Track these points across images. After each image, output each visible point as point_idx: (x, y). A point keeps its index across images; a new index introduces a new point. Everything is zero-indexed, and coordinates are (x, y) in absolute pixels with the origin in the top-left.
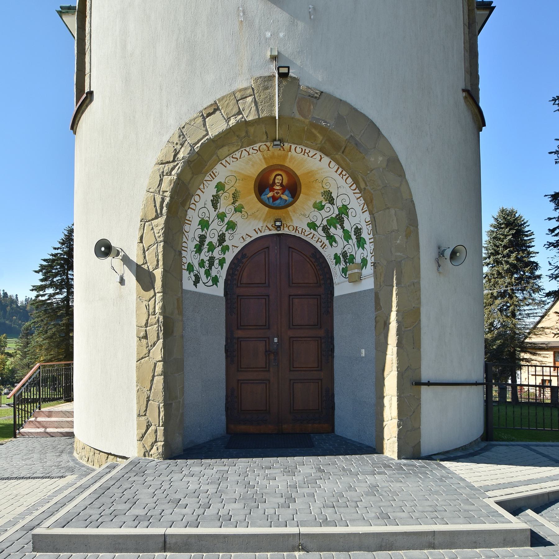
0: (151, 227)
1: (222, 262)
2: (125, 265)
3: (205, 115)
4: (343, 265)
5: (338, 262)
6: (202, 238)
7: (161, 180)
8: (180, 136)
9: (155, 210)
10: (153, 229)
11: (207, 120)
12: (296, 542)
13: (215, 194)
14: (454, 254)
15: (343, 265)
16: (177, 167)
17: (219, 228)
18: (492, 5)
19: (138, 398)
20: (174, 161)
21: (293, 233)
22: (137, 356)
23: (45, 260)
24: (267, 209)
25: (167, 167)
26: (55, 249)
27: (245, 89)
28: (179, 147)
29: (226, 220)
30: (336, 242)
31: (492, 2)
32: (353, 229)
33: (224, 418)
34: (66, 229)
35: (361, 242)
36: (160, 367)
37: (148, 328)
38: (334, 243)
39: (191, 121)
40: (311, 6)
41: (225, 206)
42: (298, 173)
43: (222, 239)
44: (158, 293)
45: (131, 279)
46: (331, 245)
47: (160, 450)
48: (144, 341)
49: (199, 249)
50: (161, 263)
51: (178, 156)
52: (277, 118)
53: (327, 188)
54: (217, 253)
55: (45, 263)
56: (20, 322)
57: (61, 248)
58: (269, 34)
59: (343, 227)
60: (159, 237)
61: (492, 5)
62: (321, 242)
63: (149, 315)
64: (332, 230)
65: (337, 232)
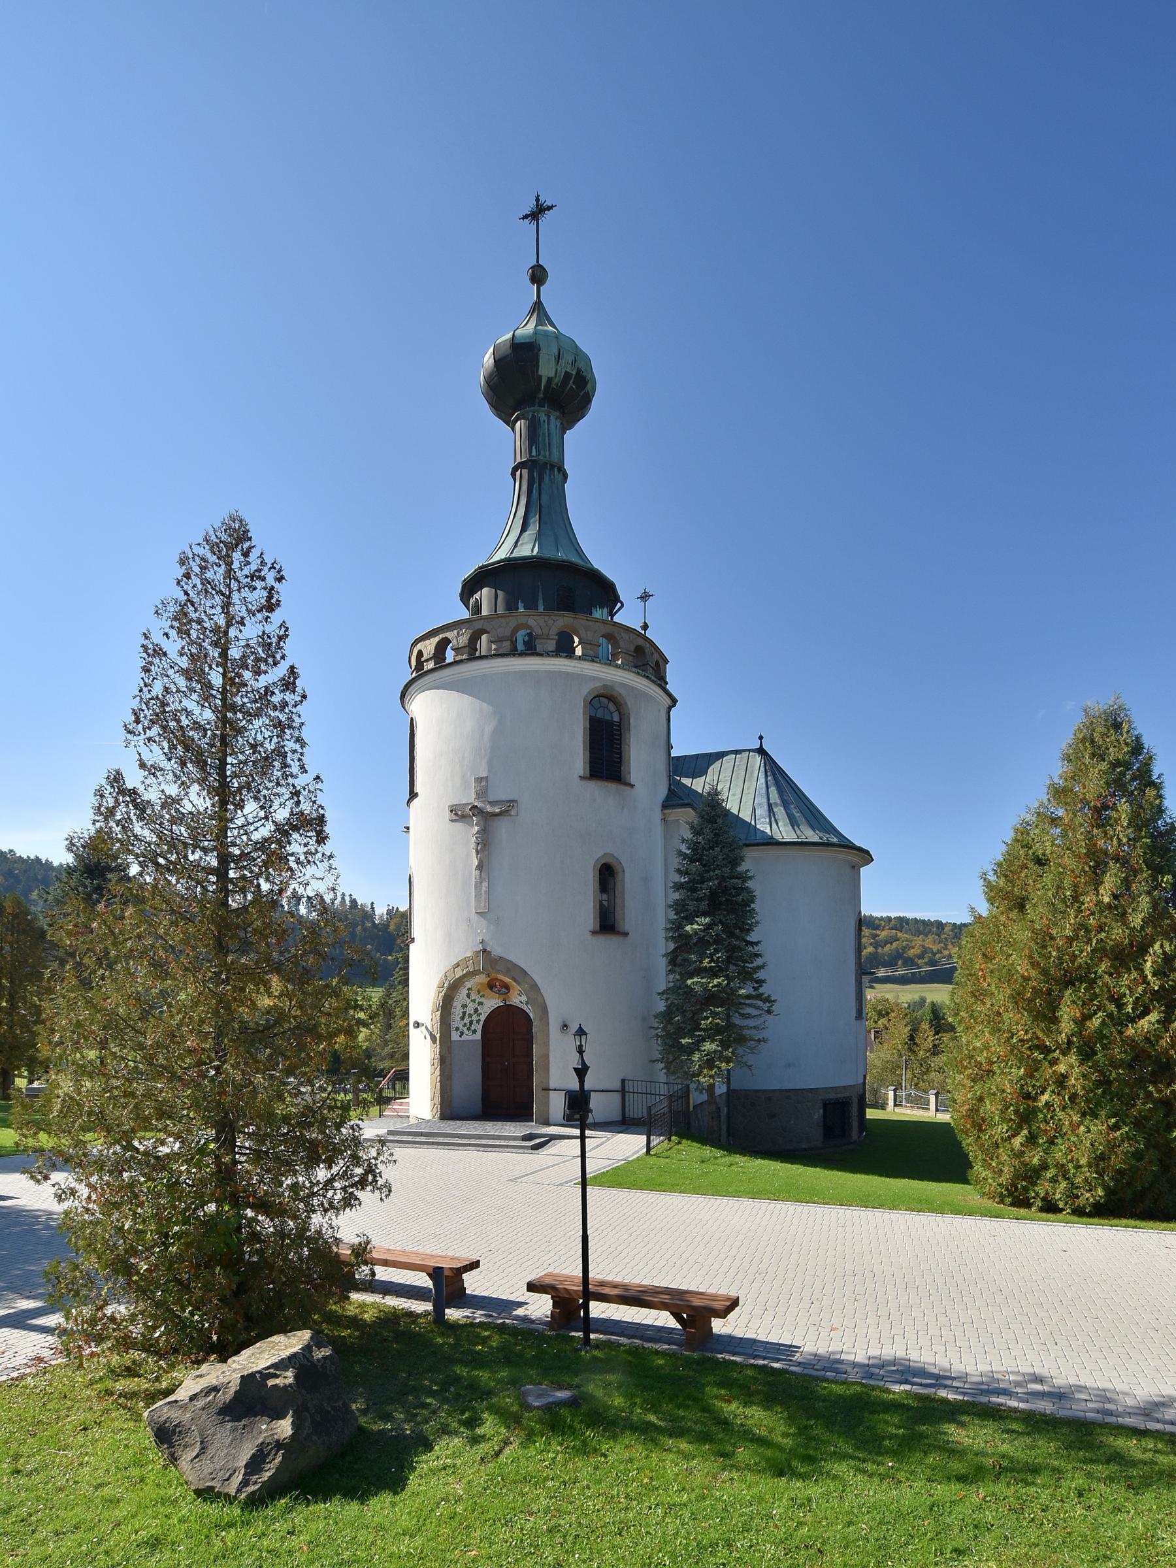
1: (478, 1022)
33: (480, 1105)
43: (476, 1010)
45: (428, 1037)
49: (462, 1018)
56: (378, 955)
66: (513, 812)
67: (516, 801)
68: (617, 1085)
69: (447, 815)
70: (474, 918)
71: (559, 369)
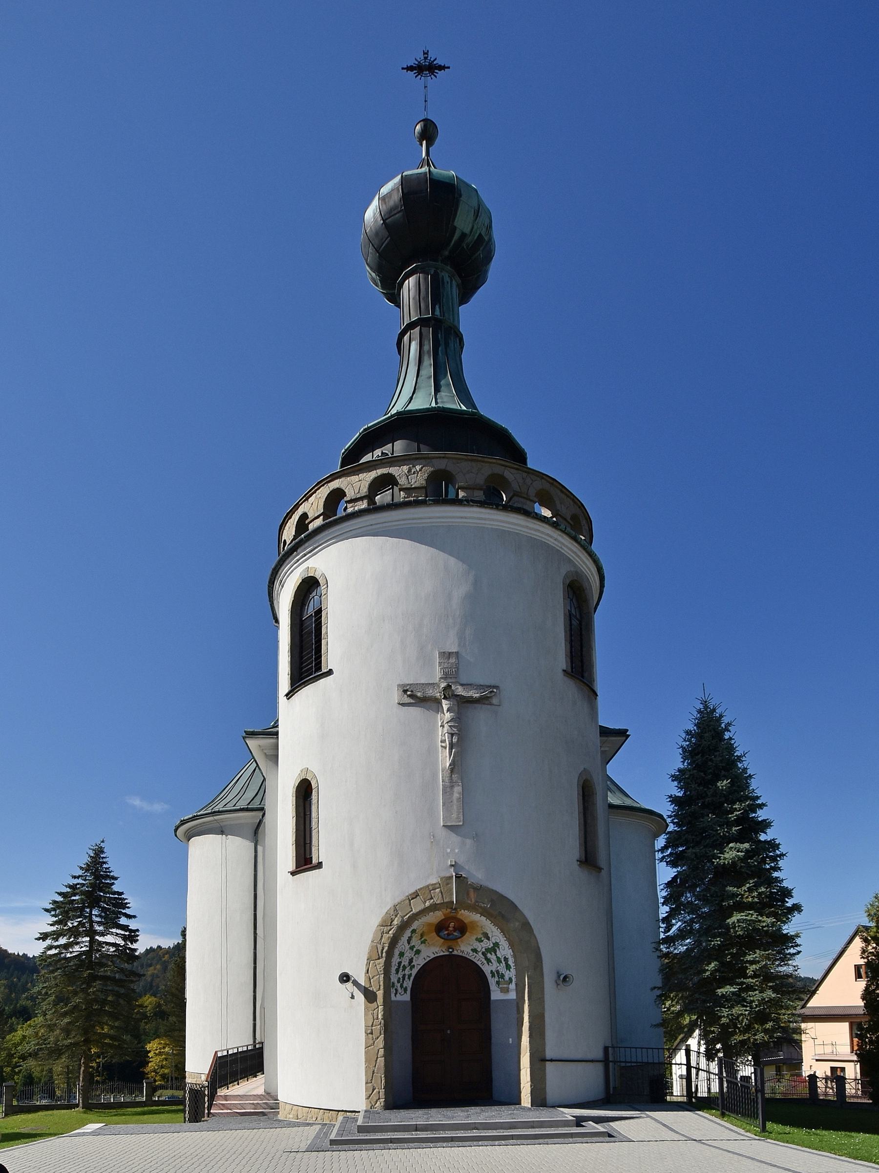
0: (375, 964)
1: (410, 976)
2: (354, 987)
3: (410, 899)
4: (496, 979)
5: (493, 976)
6: (400, 963)
7: (382, 936)
8: (394, 911)
9: (377, 954)
10: (376, 966)
11: (412, 901)
12: (474, 1126)
13: (410, 936)
14: (565, 978)
15: (496, 979)
16: (393, 929)
17: (409, 955)
18: (628, 733)
19: (366, 1072)
20: (391, 925)
21: (461, 954)
22: (365, 1046)
23: (60, 894)
24: (443, 940)
25: (386, 929)
26: (74, 877)
27: (435, 884)
28: (394, 917)
29: (415, 949)
30: (492, 963)
31: (627, 730)
32: (503, 958)
34: (92, 848)
35: (508, 967)
36: (382, 1052)
37: (373, 1028)
38: (490, 963)
39: (401, 902)
40: (474, 833)
41: (415, 942)
42: (465, 922)
43: (411, 961)
44: (380, 1006)
45: (360, 997)
46: (488, 964)
47: (382, 1104)
48: (370, 1036)
49: (397, 971)
50: (382, 987)
51: (393, 923)
52: (455, 902)
53: (485, 931)
54: (407, 972)
55: (60, 899)
57: (82, 876)
58: (449, 850)
59: (496, 955)
60: (381, 971)
61: (628, 733)
62: (481, 961)
63: (374, 1019)
64: (489, 955)
65: (492, 957)
66: (495, 701)
67: (497, 687)
68: (599, 1054)
69: (396, 696)
70: (442, 833)
71: (475, 227)
